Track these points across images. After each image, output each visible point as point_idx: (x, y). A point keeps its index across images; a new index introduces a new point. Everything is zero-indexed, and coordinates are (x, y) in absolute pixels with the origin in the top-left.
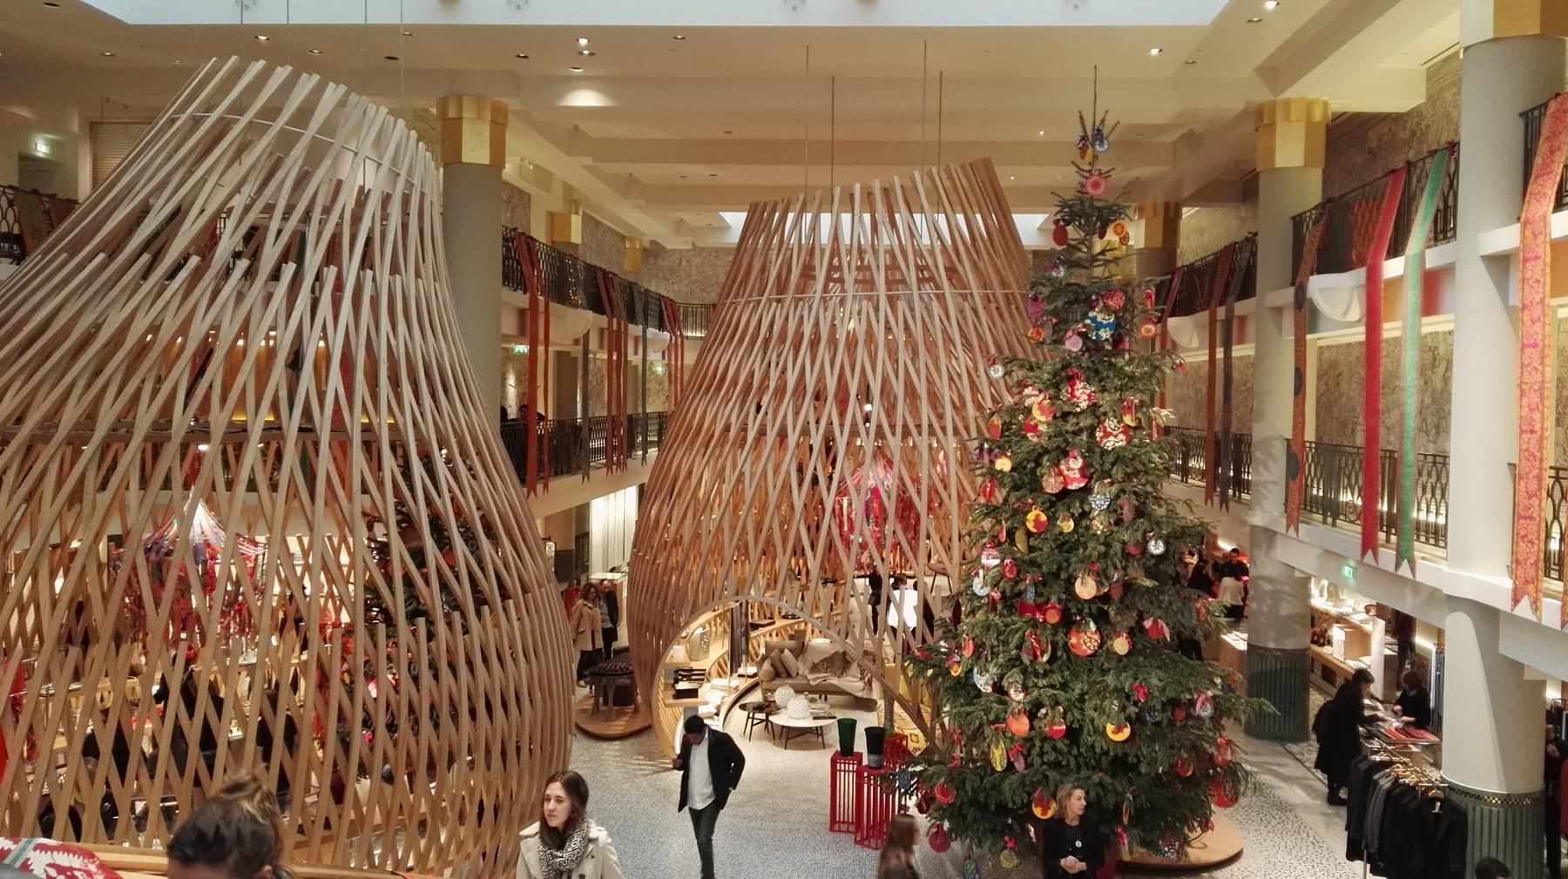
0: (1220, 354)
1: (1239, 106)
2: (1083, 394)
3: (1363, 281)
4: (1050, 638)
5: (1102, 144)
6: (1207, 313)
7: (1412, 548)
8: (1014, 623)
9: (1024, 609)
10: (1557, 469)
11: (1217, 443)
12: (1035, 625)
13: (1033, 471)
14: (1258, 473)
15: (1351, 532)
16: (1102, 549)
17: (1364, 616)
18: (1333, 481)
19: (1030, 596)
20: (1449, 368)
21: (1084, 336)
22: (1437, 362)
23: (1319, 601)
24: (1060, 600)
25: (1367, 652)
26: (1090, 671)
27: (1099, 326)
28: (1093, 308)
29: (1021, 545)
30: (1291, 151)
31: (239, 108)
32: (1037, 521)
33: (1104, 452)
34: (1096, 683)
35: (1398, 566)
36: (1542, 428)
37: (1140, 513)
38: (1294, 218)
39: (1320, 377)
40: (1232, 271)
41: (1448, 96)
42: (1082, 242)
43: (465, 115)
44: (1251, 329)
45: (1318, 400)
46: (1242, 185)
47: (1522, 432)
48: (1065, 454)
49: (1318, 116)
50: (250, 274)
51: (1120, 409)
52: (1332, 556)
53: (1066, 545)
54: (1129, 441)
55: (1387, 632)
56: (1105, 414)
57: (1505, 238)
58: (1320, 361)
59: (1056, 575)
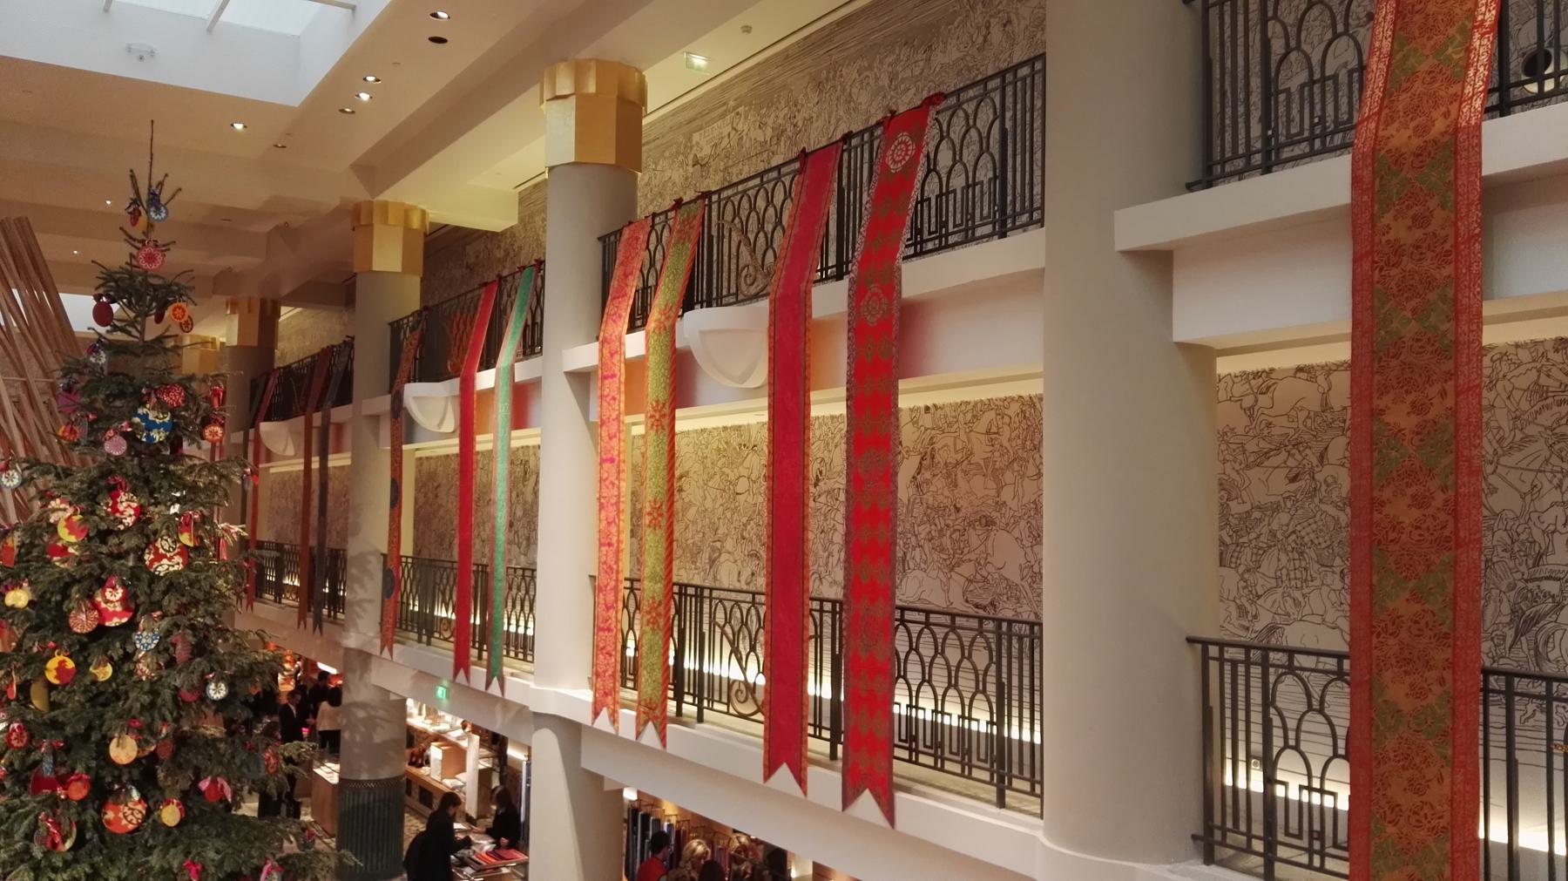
0: (315, 465)
1: (336, 202)
2: (127, 508)
3: (457, 392)
4: (74, 818)
5: (158, 211)
6: (301, 419)
7: (501, 665)
8: (23, 804)
9: (40, 783)
10: (632, 581)
11: (312, 559)
12: (53, 804)
13: (60, 604)
14: (353, 591)
15: (443, 651)
16: (146, 699)
17: (460, 732)
18: (428, 599)
19: (47, 768)
20: (537, 482)
21: (130, 438)
22: (525, 472)
23: (418, 720)
24: (88, 769)
25: (463, 770)
26: (131, 851)
27: (151, 426)
28: (143, 404)
29: (38, 702)
30: (387, 254)
32: (61, 668)
33: (154, 579)
34: (138, 865)
35: (488, 684)
36: (619, 541)
37: (201, 649)
38: (391, 324)
39: (418, 489)
40: (329, 377)
41: (538, 219)
42: (132, 323)
44: (348, 439)
45: (417, 513)
46: (339, 287)
47: (601, 545)
48: (102, 584)
49: (416, 223)
51: (174, 527)
52: (427, 678)
53: (101, 697)
54: (188, 565)
55: (482, 745)
56: (155, 533)
57: (585, 356)
58: (419, 471)
59: (86, 737)
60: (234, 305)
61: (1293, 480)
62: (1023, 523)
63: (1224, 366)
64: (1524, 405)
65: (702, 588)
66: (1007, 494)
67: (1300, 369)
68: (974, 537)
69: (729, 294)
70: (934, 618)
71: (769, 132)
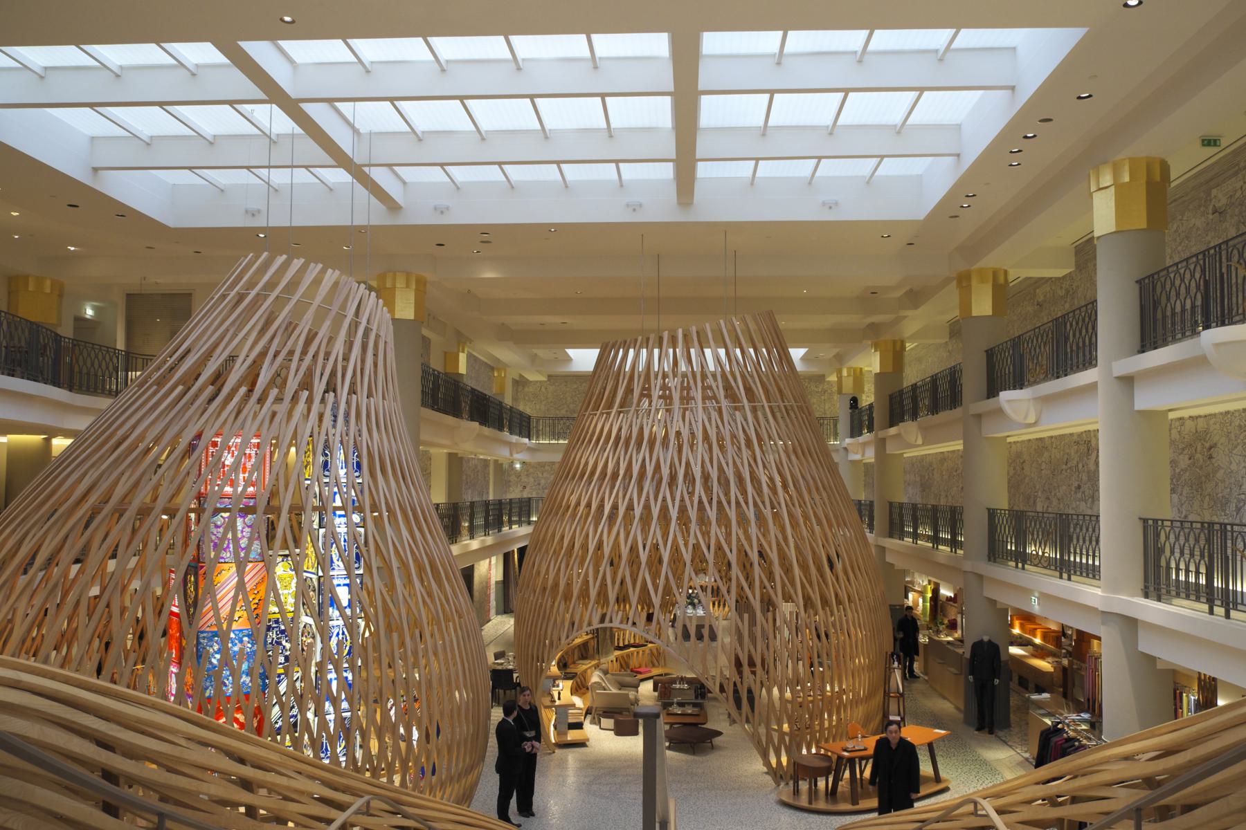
31: (271, 286)
43: (398, 285)
50: (310, 401)
60: (876, 346)
65: (1226, 525)
69: (1238, 314)
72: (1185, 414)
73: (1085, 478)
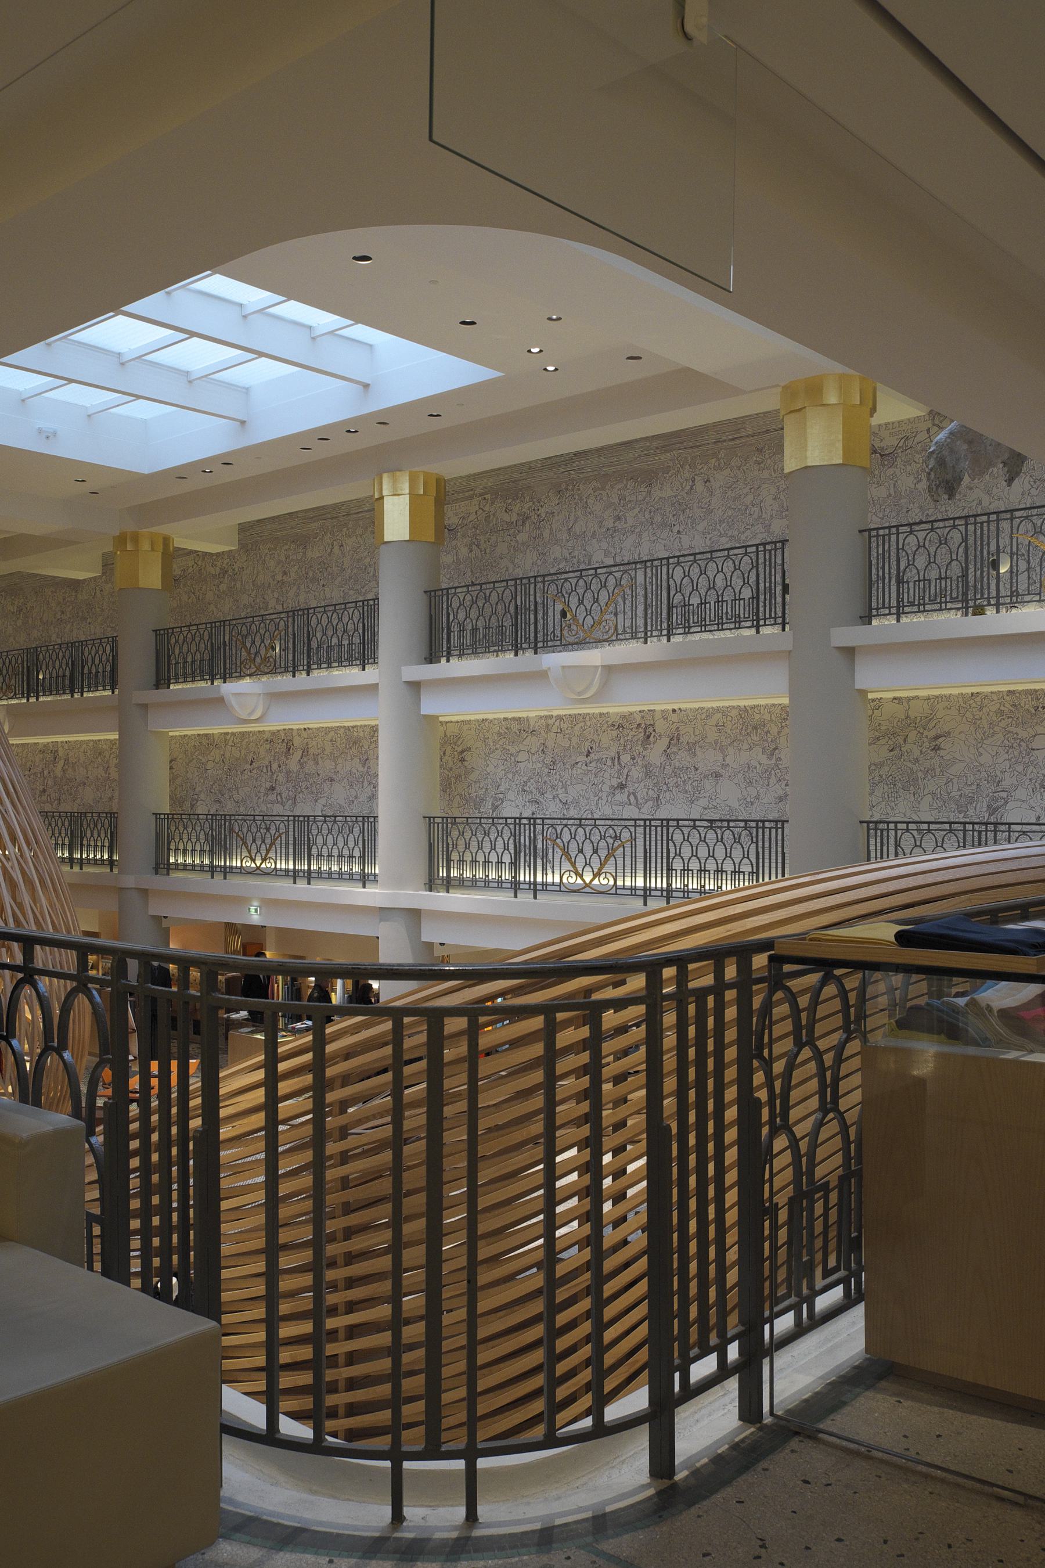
61: (891, 751)
62: (740, 775)
63: (870, 696)
64: (994, 718)
66: (339, 768)
67: (895, 698)
68: (80, 789)
70: (698, 823)
71: (218, 569)
72: (454, 719)
73: (50, 783)
